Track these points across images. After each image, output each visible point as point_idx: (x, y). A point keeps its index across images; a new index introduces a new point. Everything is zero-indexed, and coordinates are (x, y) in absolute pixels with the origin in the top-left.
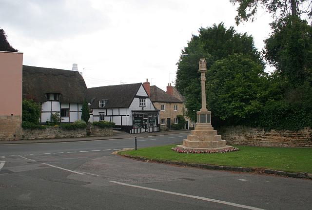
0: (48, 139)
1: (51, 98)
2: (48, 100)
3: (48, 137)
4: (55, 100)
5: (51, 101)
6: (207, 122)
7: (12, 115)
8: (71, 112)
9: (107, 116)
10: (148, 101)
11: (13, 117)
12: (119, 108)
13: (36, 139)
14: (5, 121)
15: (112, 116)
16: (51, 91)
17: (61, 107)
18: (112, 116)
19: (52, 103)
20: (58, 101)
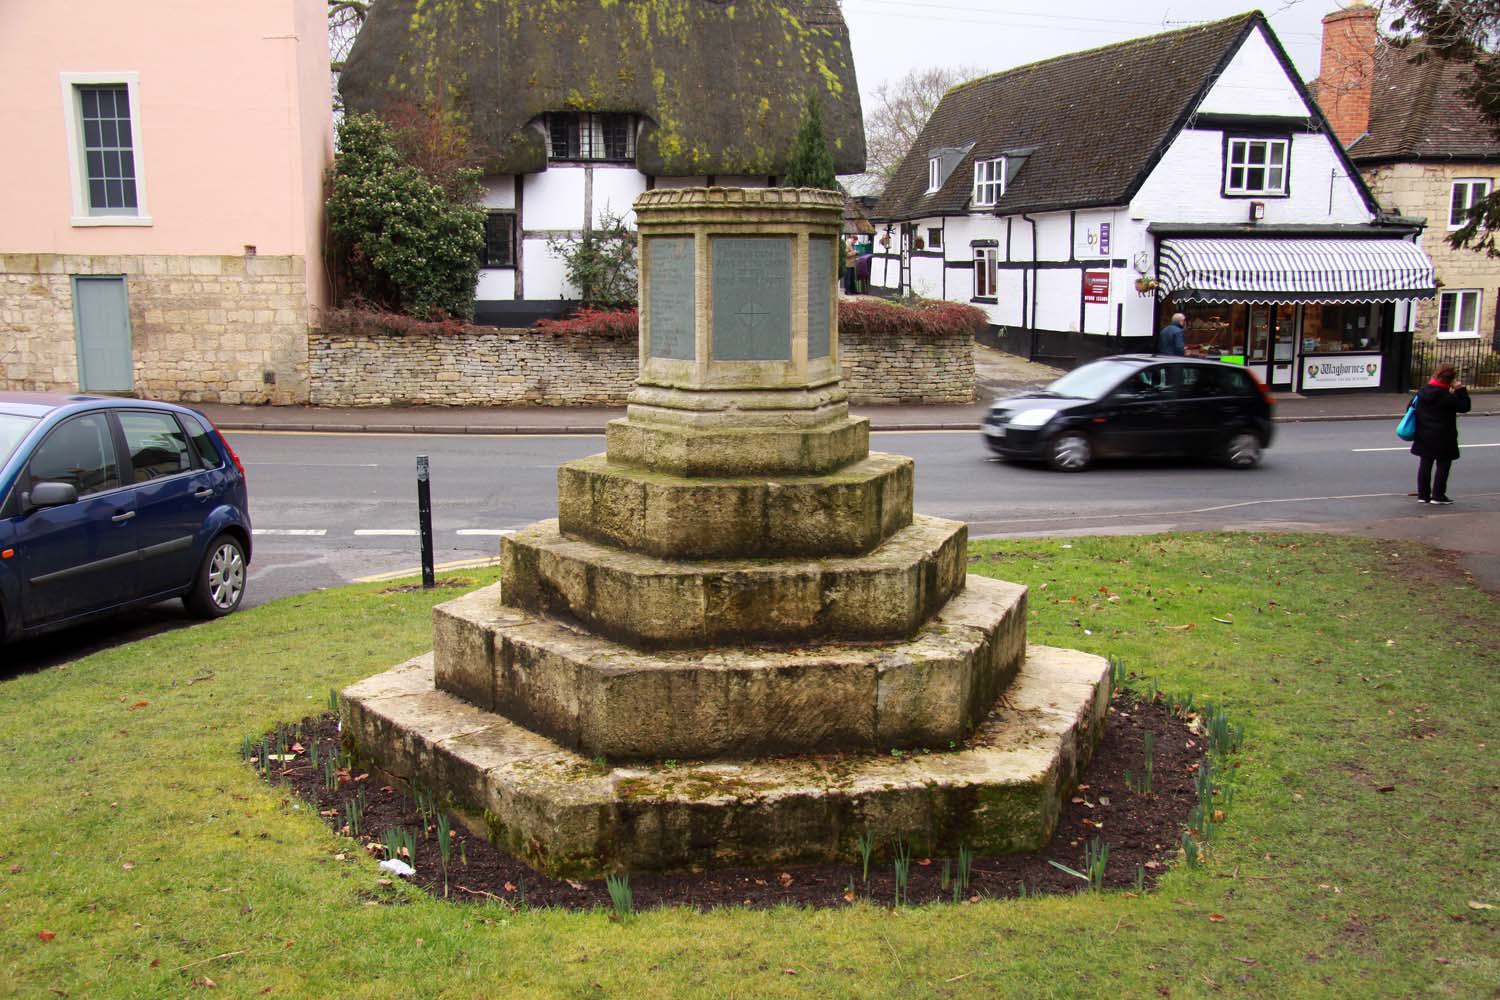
0: (478, 407)
1: (592, 142)
2: (567, 153)
3: (481, 394)
4: (615, 158)
5: (589, 162)
6: (1249, 187)
7: (251, 249)
8: (1008, 258)
9: (1009, 265)
10: (1311, 156)
11: (255, 267)
12: (1073, 209)
13: (403, 405)
14: (217, 288)
15: (1037, 265)
16: (576, 99)
17: (1408, 294)
18: (1037, 265)
19: (590, 177)
20: (631, 163)
